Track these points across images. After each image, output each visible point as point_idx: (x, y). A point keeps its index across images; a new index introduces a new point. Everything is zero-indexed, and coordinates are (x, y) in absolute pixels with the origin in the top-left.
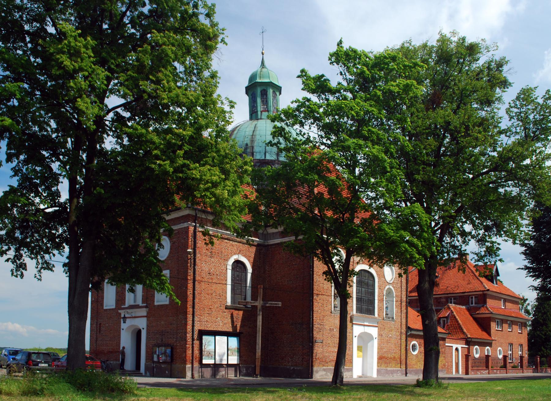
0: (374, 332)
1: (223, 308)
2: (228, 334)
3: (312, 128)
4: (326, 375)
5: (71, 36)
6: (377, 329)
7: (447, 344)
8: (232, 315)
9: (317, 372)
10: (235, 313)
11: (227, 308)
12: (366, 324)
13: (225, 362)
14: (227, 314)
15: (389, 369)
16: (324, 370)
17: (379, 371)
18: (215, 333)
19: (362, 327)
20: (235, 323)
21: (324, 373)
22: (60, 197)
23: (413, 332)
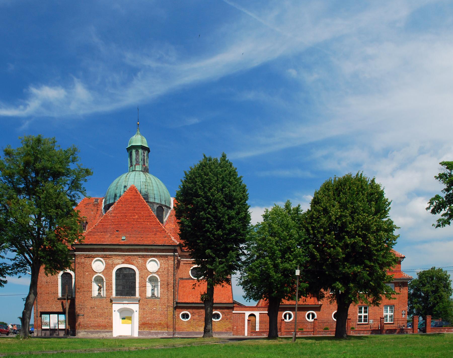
0: (135, 307)
1: (56, 299)
2: (58, 313)
3: (77, 166)
4: (87, 334)
5: (374, 250)
6: (138, 305)
7: (233, 312)
8: (62, 303)
9: (80, 332)
10: (65, 302)
11: (59, 299)
12: (124, 302)
13: (57, 328)
14: (59, 303)
15: (152, 331)
16: (85, 331)
17: (140, 333)
18: (49, 313)
19: (122, 305)
20: (65, 307)
21: (85, 333)
22: (409, 294)
23: (179, 305)
